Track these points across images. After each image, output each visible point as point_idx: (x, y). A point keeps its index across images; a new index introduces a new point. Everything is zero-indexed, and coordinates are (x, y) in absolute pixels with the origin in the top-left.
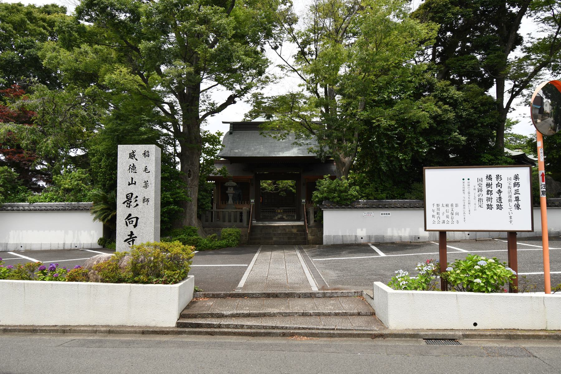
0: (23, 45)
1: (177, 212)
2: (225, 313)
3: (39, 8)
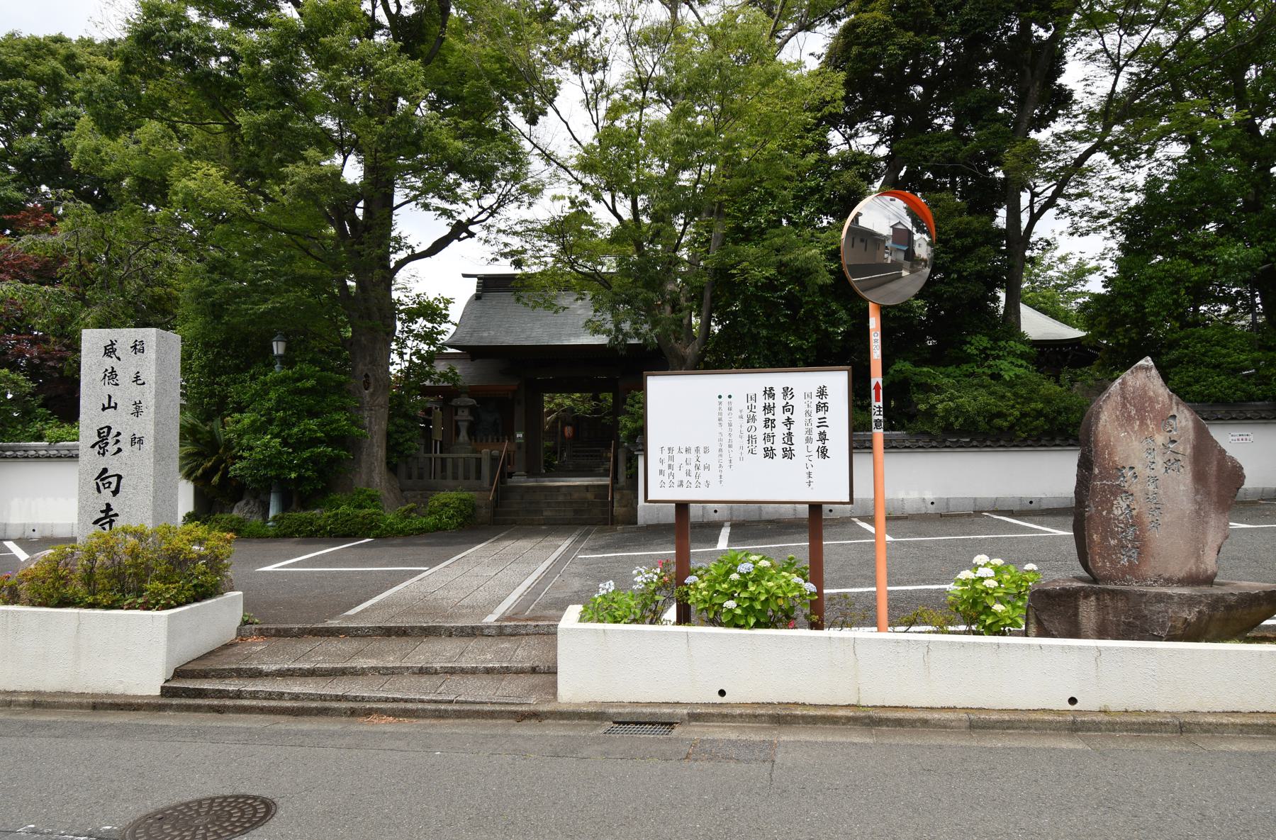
0: (57, 123)
1: (333, 461)
2: (264, 667)
3: (101, 46)
